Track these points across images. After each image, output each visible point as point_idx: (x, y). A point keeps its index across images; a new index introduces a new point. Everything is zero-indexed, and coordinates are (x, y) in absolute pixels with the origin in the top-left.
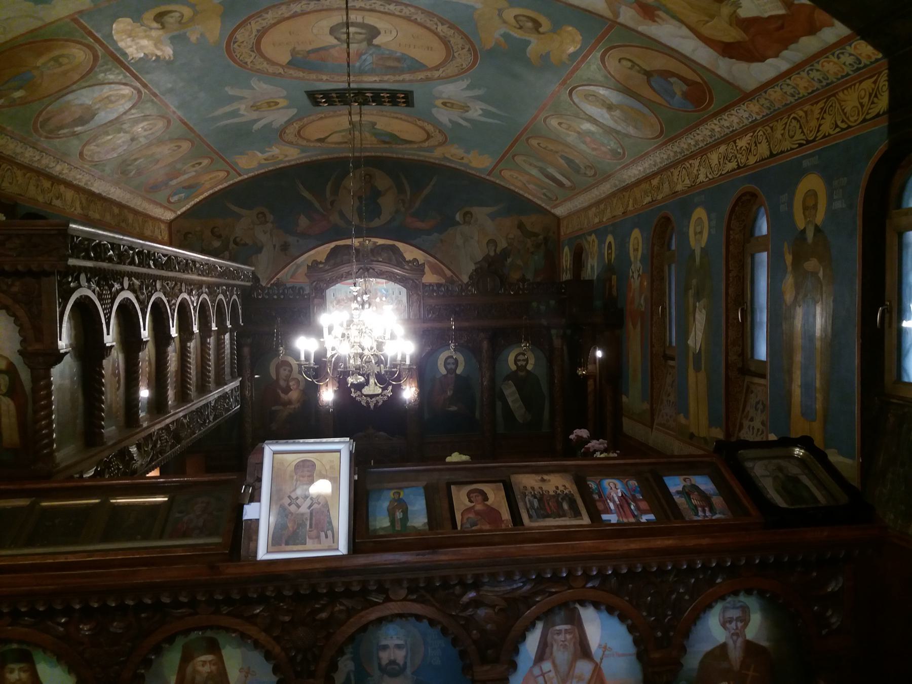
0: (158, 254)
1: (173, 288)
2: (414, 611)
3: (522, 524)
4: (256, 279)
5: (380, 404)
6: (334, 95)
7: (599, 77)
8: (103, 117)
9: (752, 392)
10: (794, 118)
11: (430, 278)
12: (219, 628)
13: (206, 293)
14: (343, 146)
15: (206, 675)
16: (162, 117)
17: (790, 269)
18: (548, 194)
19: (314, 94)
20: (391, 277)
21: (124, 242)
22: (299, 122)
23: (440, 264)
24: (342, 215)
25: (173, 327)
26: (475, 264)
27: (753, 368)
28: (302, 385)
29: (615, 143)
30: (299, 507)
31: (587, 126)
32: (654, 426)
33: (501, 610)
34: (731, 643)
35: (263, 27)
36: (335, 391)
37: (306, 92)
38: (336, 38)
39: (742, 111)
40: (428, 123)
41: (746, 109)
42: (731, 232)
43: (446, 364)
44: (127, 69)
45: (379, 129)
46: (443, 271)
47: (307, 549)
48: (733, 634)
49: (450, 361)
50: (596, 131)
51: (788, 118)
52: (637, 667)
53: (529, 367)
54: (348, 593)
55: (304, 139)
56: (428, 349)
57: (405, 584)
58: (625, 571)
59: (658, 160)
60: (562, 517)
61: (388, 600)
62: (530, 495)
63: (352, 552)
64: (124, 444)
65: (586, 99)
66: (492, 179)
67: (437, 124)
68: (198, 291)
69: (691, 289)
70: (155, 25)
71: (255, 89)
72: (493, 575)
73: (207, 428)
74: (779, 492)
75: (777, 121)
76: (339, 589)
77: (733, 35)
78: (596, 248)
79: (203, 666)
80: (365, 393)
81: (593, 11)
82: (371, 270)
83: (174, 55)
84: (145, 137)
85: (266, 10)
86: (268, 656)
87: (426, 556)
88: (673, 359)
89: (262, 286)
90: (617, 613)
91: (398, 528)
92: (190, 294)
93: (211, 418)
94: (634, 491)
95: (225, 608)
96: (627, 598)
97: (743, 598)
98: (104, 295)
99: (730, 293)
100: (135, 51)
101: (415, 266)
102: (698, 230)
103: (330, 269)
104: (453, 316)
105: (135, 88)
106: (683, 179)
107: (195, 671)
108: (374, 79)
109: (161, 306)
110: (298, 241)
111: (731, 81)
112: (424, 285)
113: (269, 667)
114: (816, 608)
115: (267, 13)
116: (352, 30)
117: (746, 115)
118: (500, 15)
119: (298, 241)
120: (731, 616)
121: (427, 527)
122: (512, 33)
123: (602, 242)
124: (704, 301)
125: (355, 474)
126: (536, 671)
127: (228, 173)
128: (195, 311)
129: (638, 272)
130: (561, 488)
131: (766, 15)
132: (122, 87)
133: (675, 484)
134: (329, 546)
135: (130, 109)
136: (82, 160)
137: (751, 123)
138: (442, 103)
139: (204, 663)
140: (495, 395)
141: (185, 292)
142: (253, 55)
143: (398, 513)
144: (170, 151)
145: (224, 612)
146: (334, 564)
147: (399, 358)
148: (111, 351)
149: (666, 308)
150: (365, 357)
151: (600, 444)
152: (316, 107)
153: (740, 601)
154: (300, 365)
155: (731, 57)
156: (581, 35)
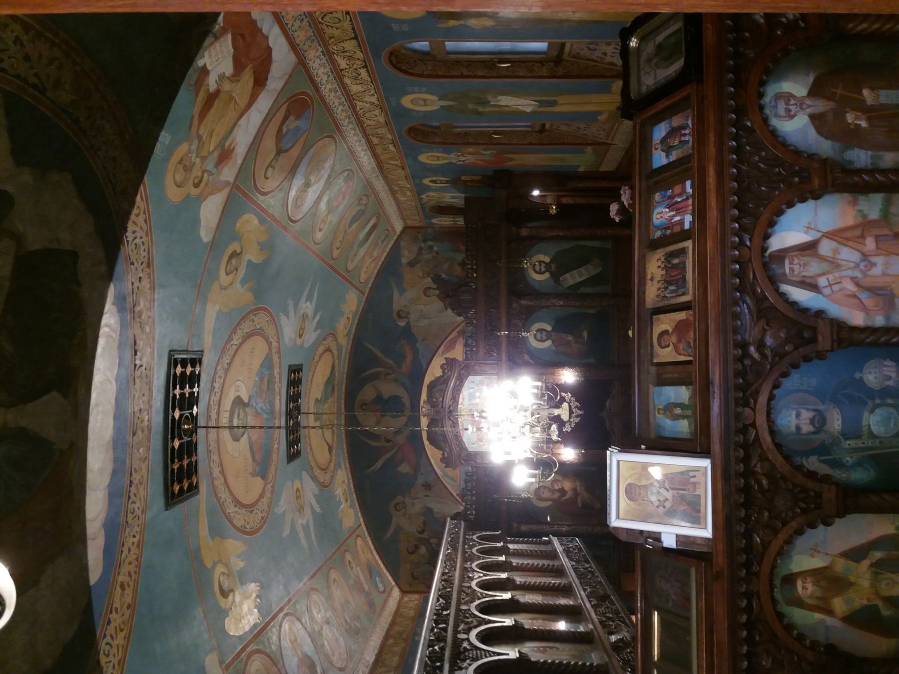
1: (467, 594)
2: (765, 402)
3: (690, 302)
4: (456, 517)
5: (578, 405)
6: (292, 437)
8: (308, 647)
10: (322, 19)
11: (458, 353)
13: (471, 564)
15: (815, 587)
16: (308, 595)
17: (462, 22)
18: (383, 238)
20: (458, 390)
24: (398, 432)
27: (556, 53)
30: (667, 500)
31: (323, 206)
32: (609, 142)
33: (767, 324)
34: (809, 110)
37: (288, 462)
38: (242, 436)
39: (314, 65)
40: (317, 350)
41: (313, 61)
42: (425, 73)
44: (268, 624)
49: (539, 336)
50: (327, 197)
51: (322, 23)
52: (827, 198)
53: (547, 260)
54: (746, 460)
55: (329, 464)
57: (740, 409)
59: (356, 138)
60: (685, 265)
61: (753, 425)
65: (299, 206)
69: (477, 109)
70: (231, 597)
71: (285, 509)
72: (736, 331)
73: (596, 570)
75: (324, 33)
76: (741, 467)
77: (248, 78)
79: (807, 589)
80: (568, 419)
82: (451, 408)
83: (256, 582)
84: (325, 612)
85: (218, 499)
86: (800, 532)
87: (716, 390)
88: (544, 125)
90: (775, 218)
91: (689, 412)
92: (472, 579)
93: (587, 565)
94: (664, 197)
95: (754, 567)
96: (762, 209)
97: (767, 99)
98: (473, 655)
99: (483, 74)
100: (253, 617)
102: (422, 102)
103: (449, 446)
105: (283, 618)
106: (374, 116)
107: (810, 597)
108: (278, 401)
109: (482, 606)
110: (422, 474)
112: (466, 359)
113: (810, 532)
114: (779, 33)
115: (221, 498)
116: (235, 424)
117: (318, 61)
118: (225, 288)
119: (422, 474)
121: (690, 387)
123: (429, 189)
124: (489, 98)
126: (827, 291)
127: (358, 536)
128: (488, 575)
129: (459, 156)
130: (659, 263)
131: (232, 50)
133: (660, 159)
134: (703, 475)
135: (301, 623)
136: (345, 669)
137: (325, 56)
138: (300, 338)
139: (804, 588)
140: (573, 294)
142: (255, 511)
144: (338, 589)
145: (758, 569)
147: (536, 391)
148: (523, 653)
149: (494, 131)
151: (625, 193)
153: (770, 102)
155: (266, 79)
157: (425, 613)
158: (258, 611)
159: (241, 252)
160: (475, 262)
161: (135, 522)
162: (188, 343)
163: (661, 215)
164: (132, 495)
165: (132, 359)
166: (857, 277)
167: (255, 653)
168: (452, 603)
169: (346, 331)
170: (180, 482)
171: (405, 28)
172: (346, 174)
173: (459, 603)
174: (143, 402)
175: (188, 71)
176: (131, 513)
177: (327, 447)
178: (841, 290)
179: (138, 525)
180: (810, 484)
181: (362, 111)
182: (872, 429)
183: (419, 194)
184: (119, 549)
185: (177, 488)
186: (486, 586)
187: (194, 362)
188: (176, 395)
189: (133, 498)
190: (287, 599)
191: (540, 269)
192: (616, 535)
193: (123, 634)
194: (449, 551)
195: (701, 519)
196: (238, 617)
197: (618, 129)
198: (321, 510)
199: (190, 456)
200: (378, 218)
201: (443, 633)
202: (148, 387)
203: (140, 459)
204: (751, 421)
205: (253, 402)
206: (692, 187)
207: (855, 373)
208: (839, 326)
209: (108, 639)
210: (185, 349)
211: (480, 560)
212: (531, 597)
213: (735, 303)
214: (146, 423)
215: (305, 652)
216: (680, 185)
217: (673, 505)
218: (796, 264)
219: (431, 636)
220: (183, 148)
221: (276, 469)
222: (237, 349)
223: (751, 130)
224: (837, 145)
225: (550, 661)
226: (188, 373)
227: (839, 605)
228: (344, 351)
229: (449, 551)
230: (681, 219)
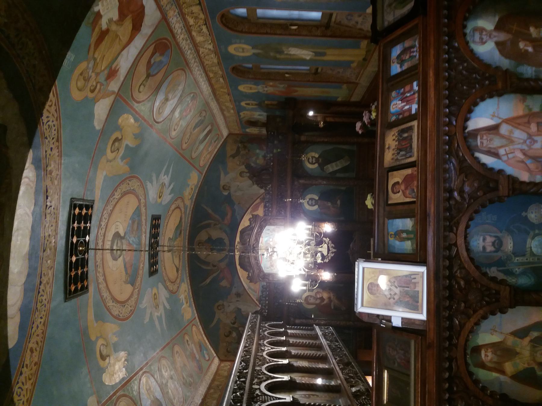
0: (239, 367)
1: (260, 360)
3: (415, 162)
4: (256, 313)
5: (333, 245)
6: (152, 260)
7: (148, 105)
8: (158, 394)
9: (340, 22)
11: (260, 212)
12: (466, 345)
13: (263, 342)
14: (181, 257)
16: (159, 361)
18: (215, 139)
20: (259, 234)
21: (232, 386)
23: (253, 205)
25: (282, 362)
26: (253, 185)
27: (326, 21)
28: (321, 290)
30: (395, 294)
31: (177, 114)
32: (357, 81)
33: (466, 177)
34: (495, 39)
36: (324, 271)
37: (150, 276)
38: (119, 257)
42: (244, 30)
43: (312, 205)
44: (131, 378)
45: (173, 236)
46: (256, 204)
47: (422, 290)
48: (490, 37)
49: (310, 202)
52: (506, 96)
53: (317, 156)
54: (450, 268)
56: (302, 215)
57: (447, 233)
59: (199, 72)
61: (455, 245)
62: (397, 156)
63: (426, 264)
64: (350, 395)
65: (161, 113)
66: (204, 172)
68: (262, 346)
70: (107, 360)
71: (146, 306)
72: (445, 180)
74: (404, 7)
76: (447, 273)
77: (128, 24)
79: (488, 356)
81: (110, 106)
84: (171, 371)
85: (102, 297)
86: (485, 317)
87: (431, 220)
88: (317, 69)
89: (260, 310)
90: (472, 107)
91: (412, 236)
92: (264, 351)
93: (337, 344)
94: (398, 93)
95: (454, 341)
96: (464, 101)
97: (468, 31)
98: (262, 399)
100: (122, 373)
101: (253, 220)
102: (241, 50)
104: (284, 199)
107: (490, 361)
108: (144, 237)
109: (270, 368)
110: (235, 287)
111: (155, 26)
112: (265, 215)
113: (491, 317)
115: (103, 296)
117: (175, 19)
118: (111, 161)
119: (235, 287)
120: (479, 38)
121: (413, 219)
122: (121, 155)
123: (244, 109)
124: (284, 49)
125: (378, 260)
126: (505, 158)
127: (193, 325)
128: (274, 348)
130: (394, 137)
131: (118, 4)
133: (396, 69)
135: (154, 378)
139: (486, 356)
140: (332, 177)
141: (262, 353)
144: (180, 358)
145: (457, 342)
147: (308, 232)
148: (295, 398)
150: (306, 252)
152: (158, 272)
154: (309, 290)
155: (141, 26)
156: (124, 114)
157: (232, 372)
158: (126, 369)
161: (42, 309)
162: (84, 194)
164: (41, 290)
165: (44, 201)
166: (524, 149)
167: (123, 397)
168: (250, 365)
169: (190, 197)
170: (76, 284)
172: (192, 95)
173: (254, 366)
174: (51, 230)
175: (87, 13)
176: (40, 302)
177: (175, 269)
178: (514, 157)
179: (45, 311)
180: (492, 285)
182: (533, 250)
183: (238, 113)
184: (31, 325)
185: (73, 288)
186: (273, 355)
187: (88, 207)
188: (75, 227)
189: (41, 292)
190: (145, 362)
191: (312, 161)
192: (360, 318)
193: (31, 382)
194: (250, 333)
195: (419, 307)
196: (112, 373)
197: (363, 74)
198: (170, 308)
199: (83, 268)
200: (212, 125)
201: (243, 384)
202: (55, 221)
203: (48, 267)
204: (454, 242)
205: (127, 236)
206: (418, 85)
207: (523, 212)
208: (513, 180)
209: (20, 385)
210: (82, 198)
211: (269, 339)
212: (301, 363)
213: (445, 162)
214: (53, 244)
215: (156, 397)
217: (400, 298)
218: (484, 139)
219: (235, 386)
220: (83, 65)
222: (118, 202)
223: (457, 50)
224: (513, 62)
225: (312, 404)
226: (83, 214)
227: (509, 367)
228: (188, 210)
229: (250, 333)
230: (410, 107)
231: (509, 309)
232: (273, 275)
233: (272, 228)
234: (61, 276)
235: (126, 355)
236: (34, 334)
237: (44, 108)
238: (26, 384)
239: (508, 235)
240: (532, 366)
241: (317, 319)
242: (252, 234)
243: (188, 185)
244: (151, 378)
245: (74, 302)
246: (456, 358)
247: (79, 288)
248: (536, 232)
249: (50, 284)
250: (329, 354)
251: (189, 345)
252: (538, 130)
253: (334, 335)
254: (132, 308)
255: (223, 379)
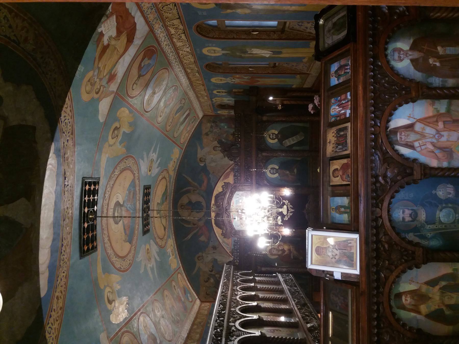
1: (234, 303)
3: (349, 154)
4: (229, 263)
5: (292, 206)
6: (145, 222)
8: (153, 330)
10: (162, 8)
11: (231, 180)
12: (390, 292)
13: (236, 287)
15: (411, 299)
16: (153, 303)
17: (234, 11)
18: (193, 120)
19: (144, 231)
20: (230, 198)
21: (214, 324)
22: (156, 239)
24: (200, 220)
27: (282, 27)
29: (170, 90)
30: (336, 255)
31: (162, 104)
32: (308, 72)
33: (388, 166)
34: (410, 57)
35: (114, 255)
40: (158, 178)
41: (157, 30)
42: (215, 37)
47: (356, 253)
48: (406, 56)
49: (272, 172)
51: (162, 11)
52: (419, 102)
53: (276, 133)
54: (377, 235)
57: (374, 209)
58: (373, 108)
59: (179, 69)
61: (381, 217)
64: (306, 330)
67: (158, 174)
70: (113, 304)
72: (372, 169)
74: (339, 34)
75: (163, 16)
76: (375, 238)
77: (124, 38)
78: (219, 99)
79: (407, 300)
80: (286, 214)
82: (227, 208)
84: (162, 311)
85: (107, 254)
86: (404, 272)
88: (275, 64)
90: (393, 112)
91: (348, 210)
92: (237, 295)
93: (296, 288)
94: (336, 100)
95: (381, 289)
96: (386, 107)
97: (389, 52)
100: (125, 314)
102: (213, 52)
106: (188, 58)
107: (409, 304)
108: (138, 204)
109: (242, 309)
110: (212, 241)
111: (144, 38)
112: (235, 183)
115: (108, 253)
116: (116, 215)
117: (160, 30)
118: (111, 146)
119: (212, 241)
120: (397, 57)
121: (349, 197)
123: (216, 96)
124: (248, 50)
126: (419, 149)
127: (179, 273)
129: (232, 79)
130: (334, 134)
131: (116, 24)
132: (140, 320)
133: (334, 81)
135: (150, 317)
137: (163, 28)
139: (406, 300)
140: (289, 149)
142: (126, 260)
143: (342, 210)
146: (363, 241)
147: (270, 199)
148: (263, 333)
150: (269, 215)
151: (316, 99)
153: (391, 53)
155: (134, 38)
159: (120, 127)
160: (239, 133)
162: (92, 173)
163: (335, 110)
164: (63, 251)
166: (434, 142)
167: (126, 333)
168: (227, 307)
170: (88, 245)
171: (205, 13)
173: (230, 308)
174: (69, 204)
175: (93, 34)
176: (62, 260)
178: (426, 148)
180: (409, 247)
181: (182, 55)
182: (441, 220)
185: (86, 248)
189: (63, 253)
190: (142, 305)
191: (273, 137)
193: (58, 322)
194: (225, 281)
197: (312, 67)
199: (93, 231)
201: (222, 322)
203: (67, 233)
204: (379, 215)
205: (125, 204)
206: (351, 95)
208: (425, 168)
209: (50, 325)
212: (267, 304)
213: (372, 155)
216: (345, 95)
217: (339, 258)
220: (91, 74)
221: (137, 239)
222: (117, 177)
223: (381, 67)
224: (424, 75)
226: (92, 189)
227: (423, 308)
229: (225, 281)
231: (423, 265)
232: (242, 232)
233: (241, 193)
234: (77, 239)
235: (127, 299)
236: (58, 285)
237: (62, 110)
238: (54, 325)
239: (422, 208)
240: (442, 307)
241: (279, 268)
242: (225, 198)
243: (172, 159)
244: (147, 317)
245: (87, 259)
246: (383, 302)
247: (90, 248)
248: (443, 206)
249: (69, 246)
250: (289, 297)
251: (175, 289)
252: (444, 127)
253: (293, 281)
254: (131, 262)
255: (203, 317)
